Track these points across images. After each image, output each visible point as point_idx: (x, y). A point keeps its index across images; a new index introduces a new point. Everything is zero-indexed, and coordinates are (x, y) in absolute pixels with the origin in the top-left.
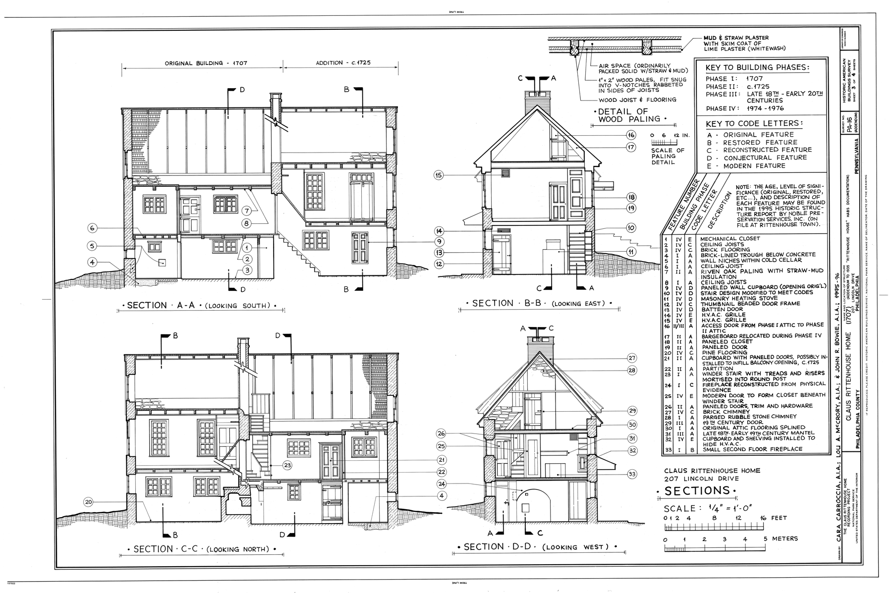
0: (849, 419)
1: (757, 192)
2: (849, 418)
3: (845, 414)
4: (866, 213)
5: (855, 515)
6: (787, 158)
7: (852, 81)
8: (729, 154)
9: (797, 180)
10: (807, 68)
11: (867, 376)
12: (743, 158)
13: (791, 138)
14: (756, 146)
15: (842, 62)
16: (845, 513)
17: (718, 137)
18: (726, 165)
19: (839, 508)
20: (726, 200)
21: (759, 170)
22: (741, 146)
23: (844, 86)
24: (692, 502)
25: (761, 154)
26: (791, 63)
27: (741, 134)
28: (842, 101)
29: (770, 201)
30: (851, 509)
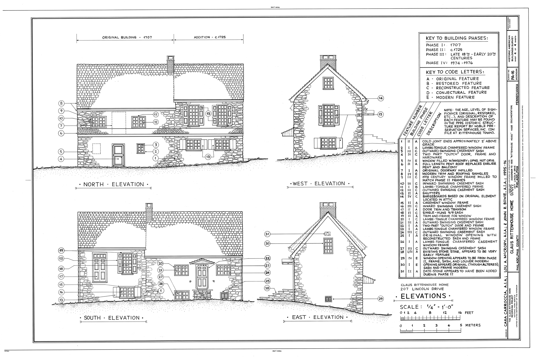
0: (512, 252)
1: (457, 114)
2: (512, 252)
3: (510, 249)
4: (522, 129)
5: (516, 310)
6: (475, 92)
7: (514, 49)
8: (439, 90)
9: (481, 106)
10: (487, 38)
11: (523, 226)
12: (448, 92)
13: (478, 81)
14: (456, 86)
15: (508, 38)
16: (510, 308)
17: (433, 81)
18: (438, 97)
19: (505, 306)
20: (438, 117)
21: (458, 99)
22: (447, 85)
23: (509, 52)
24: (417, 303)
25: (459, 90)
26: (477, 35)
27: (447, 78)
28: (508, 61)
29: (463, 118)
30: (514, 307)
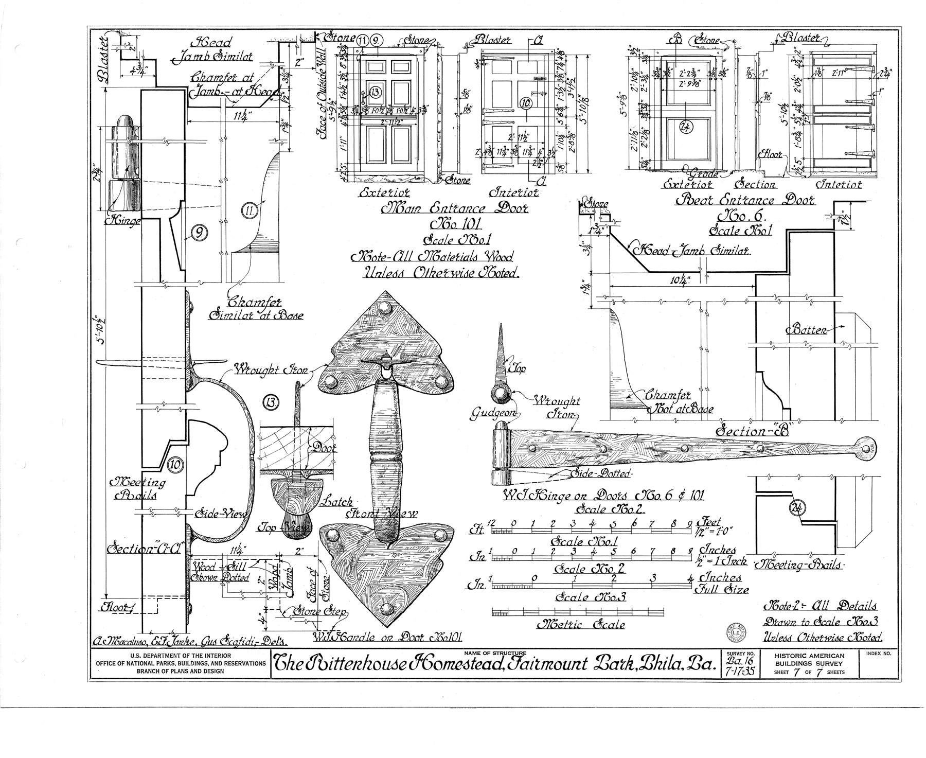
7: (808, 668)
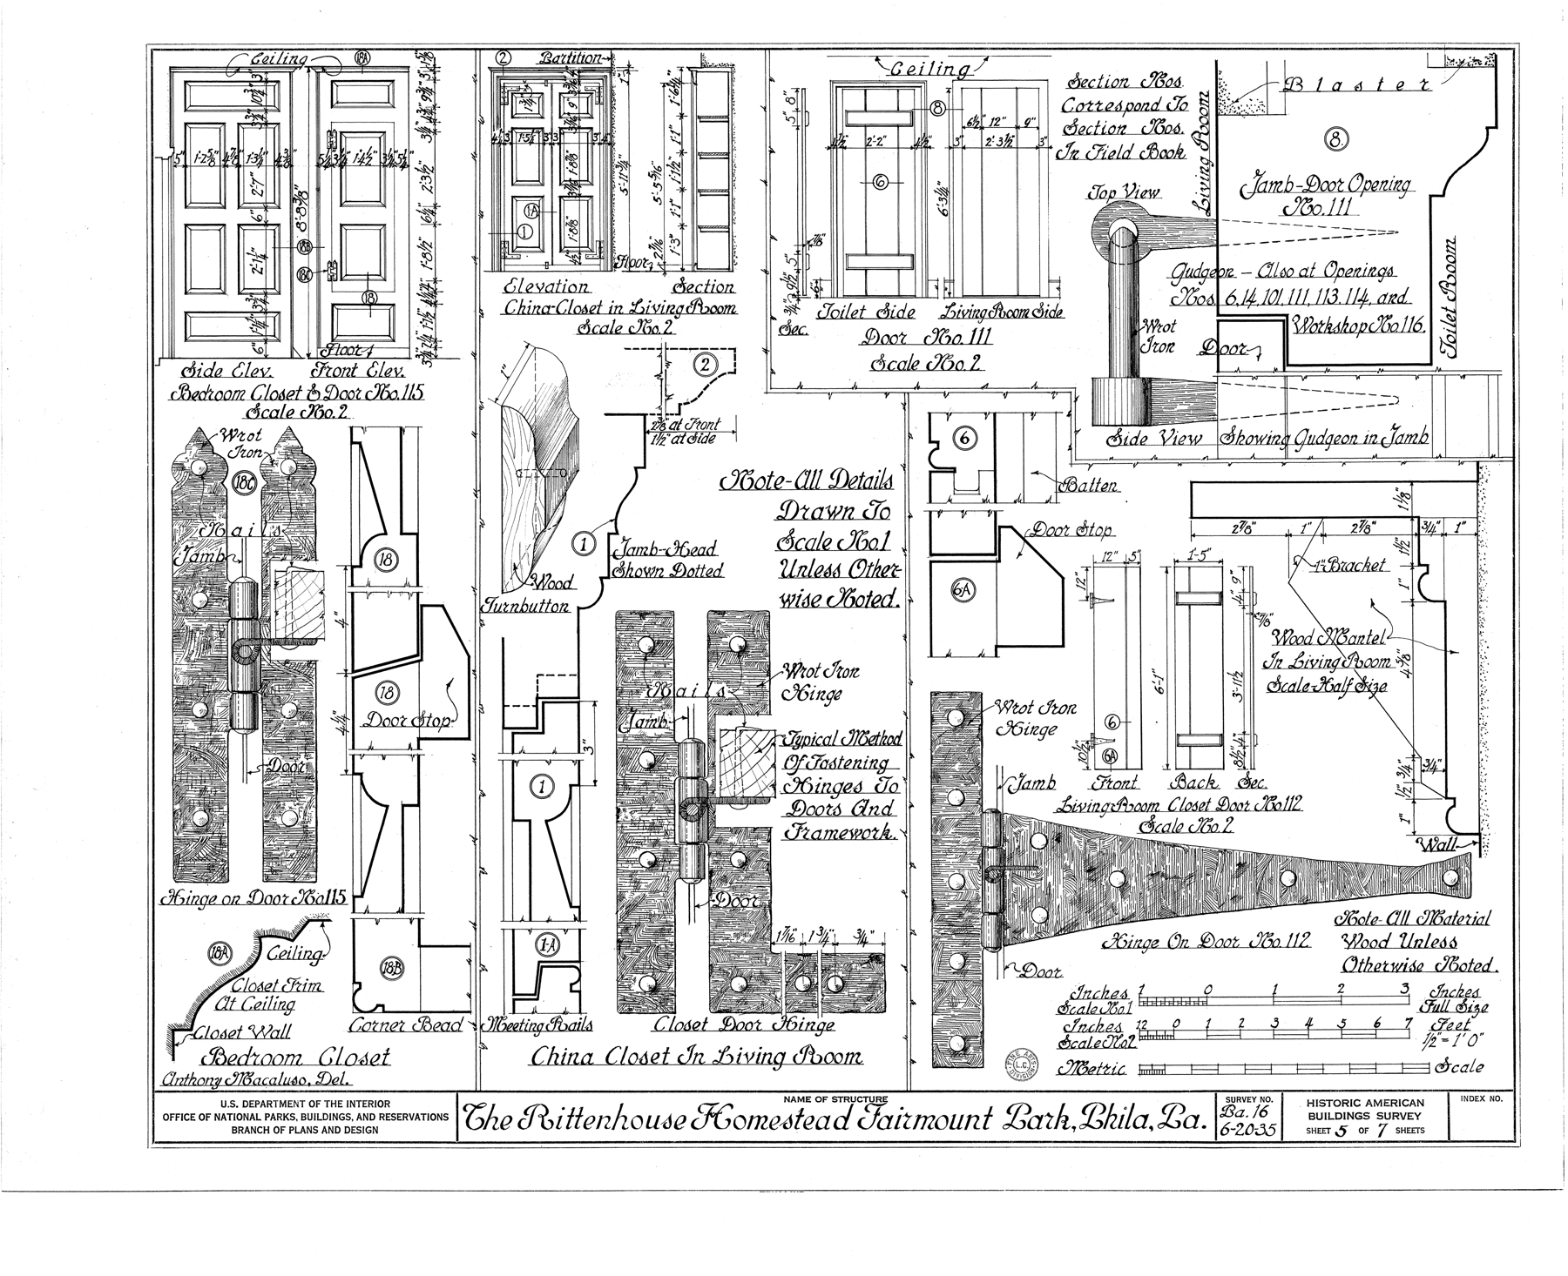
7: (1363, 1123)
